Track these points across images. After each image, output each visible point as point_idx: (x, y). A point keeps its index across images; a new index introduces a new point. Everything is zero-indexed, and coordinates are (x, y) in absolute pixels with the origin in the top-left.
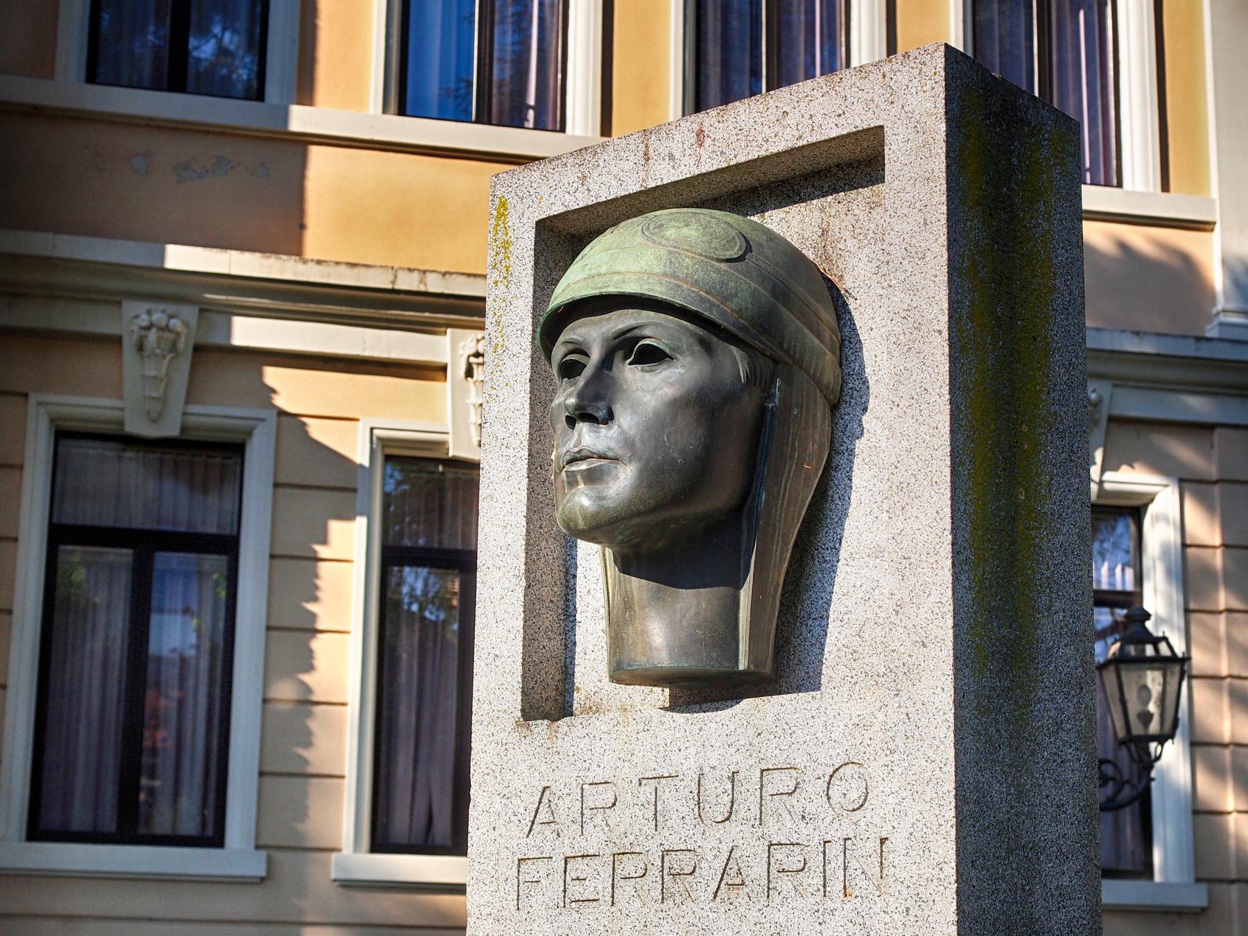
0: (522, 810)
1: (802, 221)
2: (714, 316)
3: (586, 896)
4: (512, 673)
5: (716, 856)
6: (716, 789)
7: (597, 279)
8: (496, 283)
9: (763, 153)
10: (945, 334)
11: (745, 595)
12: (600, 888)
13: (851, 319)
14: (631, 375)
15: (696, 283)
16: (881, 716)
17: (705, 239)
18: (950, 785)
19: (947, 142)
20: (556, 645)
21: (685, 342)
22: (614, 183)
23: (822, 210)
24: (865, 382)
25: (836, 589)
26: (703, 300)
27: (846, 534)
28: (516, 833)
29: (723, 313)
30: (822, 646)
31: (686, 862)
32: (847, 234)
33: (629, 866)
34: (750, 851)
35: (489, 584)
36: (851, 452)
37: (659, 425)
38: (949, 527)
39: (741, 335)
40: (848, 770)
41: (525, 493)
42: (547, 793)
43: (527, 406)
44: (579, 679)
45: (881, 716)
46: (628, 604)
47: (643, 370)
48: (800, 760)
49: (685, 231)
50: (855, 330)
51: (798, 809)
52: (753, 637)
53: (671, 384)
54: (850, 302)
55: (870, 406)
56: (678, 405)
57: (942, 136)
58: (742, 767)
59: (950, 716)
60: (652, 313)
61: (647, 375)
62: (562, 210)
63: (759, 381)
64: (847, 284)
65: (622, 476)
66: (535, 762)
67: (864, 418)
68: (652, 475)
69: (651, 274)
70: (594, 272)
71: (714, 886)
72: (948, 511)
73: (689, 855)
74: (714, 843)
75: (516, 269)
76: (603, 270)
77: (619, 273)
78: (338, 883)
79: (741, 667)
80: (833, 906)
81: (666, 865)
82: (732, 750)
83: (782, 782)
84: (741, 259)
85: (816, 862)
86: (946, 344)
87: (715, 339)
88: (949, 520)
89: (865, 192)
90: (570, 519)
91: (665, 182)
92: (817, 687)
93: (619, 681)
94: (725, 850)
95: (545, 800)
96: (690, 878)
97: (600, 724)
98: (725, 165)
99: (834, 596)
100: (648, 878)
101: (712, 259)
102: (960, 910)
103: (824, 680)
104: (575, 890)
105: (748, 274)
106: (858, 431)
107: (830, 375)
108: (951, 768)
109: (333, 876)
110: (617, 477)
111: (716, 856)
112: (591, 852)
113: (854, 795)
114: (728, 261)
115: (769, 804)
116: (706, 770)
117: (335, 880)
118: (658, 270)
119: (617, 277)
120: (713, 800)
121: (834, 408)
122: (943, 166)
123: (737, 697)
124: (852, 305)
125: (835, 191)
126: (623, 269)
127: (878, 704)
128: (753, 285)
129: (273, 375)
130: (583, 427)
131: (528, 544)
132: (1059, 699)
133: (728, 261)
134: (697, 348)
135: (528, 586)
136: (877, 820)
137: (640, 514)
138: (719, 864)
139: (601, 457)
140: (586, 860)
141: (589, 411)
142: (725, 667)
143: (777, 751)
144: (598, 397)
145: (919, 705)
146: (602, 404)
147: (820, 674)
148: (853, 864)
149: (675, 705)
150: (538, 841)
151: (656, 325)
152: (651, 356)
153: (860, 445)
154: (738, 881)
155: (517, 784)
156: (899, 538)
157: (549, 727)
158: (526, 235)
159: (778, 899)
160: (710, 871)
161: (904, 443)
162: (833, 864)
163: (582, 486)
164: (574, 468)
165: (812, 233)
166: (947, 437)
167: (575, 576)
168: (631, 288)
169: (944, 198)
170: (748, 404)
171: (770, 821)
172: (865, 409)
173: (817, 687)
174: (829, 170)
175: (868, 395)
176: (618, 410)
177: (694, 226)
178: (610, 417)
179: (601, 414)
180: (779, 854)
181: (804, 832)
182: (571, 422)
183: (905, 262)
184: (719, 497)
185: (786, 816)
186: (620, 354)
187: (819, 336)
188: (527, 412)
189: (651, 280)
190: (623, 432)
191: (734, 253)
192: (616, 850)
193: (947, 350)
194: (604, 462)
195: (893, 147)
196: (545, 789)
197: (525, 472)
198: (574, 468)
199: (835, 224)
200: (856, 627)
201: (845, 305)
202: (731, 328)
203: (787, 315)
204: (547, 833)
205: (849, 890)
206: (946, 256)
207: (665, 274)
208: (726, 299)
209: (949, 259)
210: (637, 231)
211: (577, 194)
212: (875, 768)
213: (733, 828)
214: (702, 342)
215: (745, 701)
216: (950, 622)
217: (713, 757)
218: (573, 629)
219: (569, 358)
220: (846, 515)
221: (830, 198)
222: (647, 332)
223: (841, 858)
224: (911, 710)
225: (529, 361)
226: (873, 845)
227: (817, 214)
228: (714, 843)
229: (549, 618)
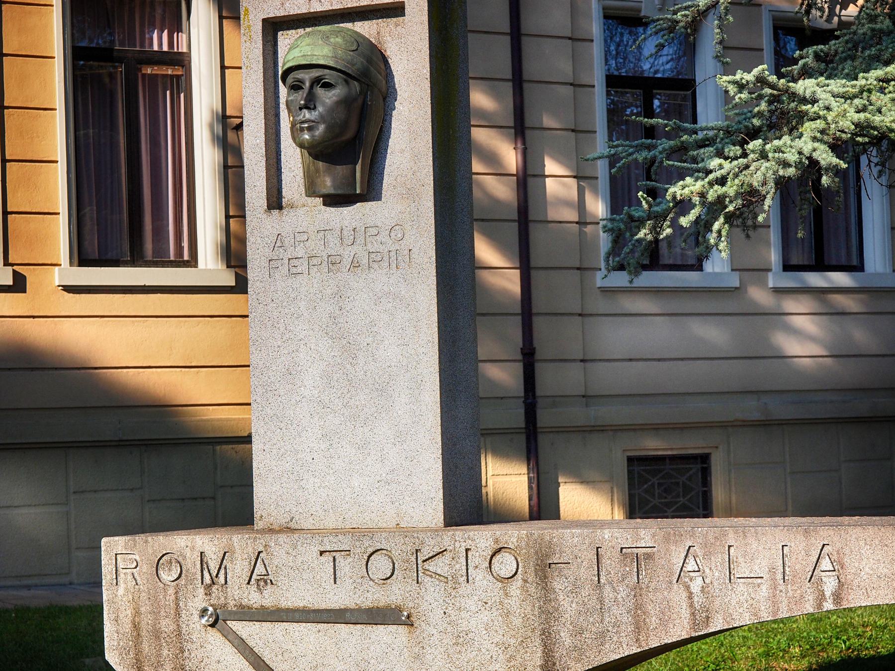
0: (269, 242)
1: (370, 28)
2: (350, 72)
3: (298, 272)
4: (262, 192)
5: (349, 257)
6: (347, 233)
7: (307, 57)
8: (245, 41)
9: (358, 5)
10: (429, 79)
11: (358, 168)
12: (303, 269)
13: (390, 66)
14: (320, 91)
15: (343, 60)
16: (408, 209)
17: (345, 42)
18: (433, 232)
19: (428, 10)
20: (275, 181)
21: (340, 81)
22: (296, 8)
23: (377, 24)
24: (396, 90)
25: (386, 163)
26: (346, 66)
27: (390, 144)
28: (267, 251)
29: (353, 71)
30: (382, 183)
31: (338, 259)
32: (387, 35)
33: (315, 261)
34: (362, 255)
35: (250, 159)
36: (391, 115)
37: (331, 110)
38: (431, 146)
39: (359, 78)
40: (397, 227)
41: (264, 125)
42: (280, 236)
43: (263, 91)
44: (284, 194)
45: (408, 209)
46: (317, 170)
47: (325, 90)
48: (379, 224)
49: (337, 39)
50: (391, 70)
51: (379, 240)
52: (362, 182)
53: (336, 96)
54: (389, 60)
55: (398, 99)
56: (338, 103)
57: (426, 8)
58: (358, 226)
59: (433, 209)
60: (328, 71)
61: (327, 92)
62: (274, 16)
63: (363, 93)
64: (388, 53)
65: (320, 129)
66: (273, 225)
67: (396, 103)
68: (329, 128)
69: (328, 57)
70: (305, 54)
71: (348, 267)
72: (431, 141)
73: (338, 257)
74: (348, 252)
75: (254, 37)
76: (309, 53)
77: (316, 55)
78: (61, 288)
79: (358, 192)
80: (393, 272)
81: (330, 260)
82: (354, 220)
83: (374, 231)
84: (357, 50)
85: (386, 258)
86: (429, 83)
87: (349, 79)
88: (431, 144)
89: (395, 19)
90: (302, 143)
91: (318, 10)
92: (379, 199)
93: (309, 196)
94: (352, 254)
95: (279, 239)
96: (339, 265)
97: (301, 211)
98: (342, 7)
99: (386, 166)
100: (323, 265)
101: (350, 51)
102: (437, 272)
103: (383, 195)
104: (294, 270)
105: (359, 55)
106: (393, 107)
107: (384, 89)
108: (433, 226)
109: (57, 284)
110: (318, 129)
111: (349, 257)
112: (299, 257)
113: (399, 235)
114: (353, 51)
115: (368, 240)
116: (344, 227)
117: (59, 286)
118: (330, 55)
119: (315, 57)
120: (347, 238)
121: (384, 99)
122: (427, 19)
123: (355, 202)
124: (390, 61)
125: (382, 18)
126: (317, 54)
127: (407, 205)
128: (362, 59)
129: (825, 354)
130: (305, 111)
131: (265, 144)
132: (463, 201)
133: (353, 51)
134: (344, 83)
135: (267, 160)
136: (408, 243)
137: (326, 141)
138: (350, 260)
139: (313, 121)
140: (297, 260)
141: (309, 106)
142: (353, 192)
143: (371, 221)
144: (310, 101)
145: (422, 206)
146: (312, 103)
147: (382, 193)
148: (400, 258)
149: (324, 204)
150: (277, 253)
151: (330, 75)
152: (327, 86)
153: (394, 113)
154: (357, 265)
155: (266, 233)
156: (414, 149)
157: (279, 212)
158: (258, 24)
159: (373, 271)
160: (347, 262)
161: (415, 116)
162: (392, 258)
163: (306, 132)
164: (303, 126)
165: (374, 32)
166: (430, 115)
167: (280, 155)
168: (322, 62)
169: (428, 31)
170: (360, 101)
171: (369, 245)
172: (396, 100)
173: (379, 199)
174: (380, 9)
175: (397, 95)
176: (318, 105)
177: (340, 37)
178: (315, 108)
179: (312, 107)
180: (372, 256)
181: (381, 248)
182: (301, 109)
183: (414, 52)
184: (350, 134)
185: (375, 242)
186: (316, 84)
187: (381, 75)
188: (263, 94)
189: (328, 59)
190: (320, 113)
191: (354, 48)
192: (309, 256)
193: (429, 85)
194: (313, 124)
195: (409, 10)
196: (279, 234)
197: (263, 117)
198: (303, 126)
199: (382, 30)
200: (395, 177)
201: (387, 61)
202: (356, 76)
203: (372, 69)
204: (281, 250)
205: (398, 267)
206: (428, 52)
207: (333, 57)
208: (353, 65)
209: (430, 53)
210: (319, 38)
211: (280, 10)
212: (408, 227)
213: (355, 247)
214: (346, 81)
215: (358, 204)
216: (432, 178)
217: (346, 223)
218: (281, 175)
219: (295, 83)
220: (390, 137)
221: (380, 20)
222: (327, 77)
223: (395, 257)
224: (419, 207)
225: (262, 74)
226: (406, 252)
227: (375, 25)
228: (348, 252)
229: (273, 171)
